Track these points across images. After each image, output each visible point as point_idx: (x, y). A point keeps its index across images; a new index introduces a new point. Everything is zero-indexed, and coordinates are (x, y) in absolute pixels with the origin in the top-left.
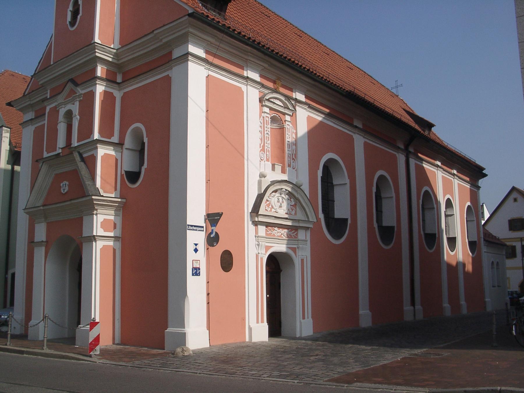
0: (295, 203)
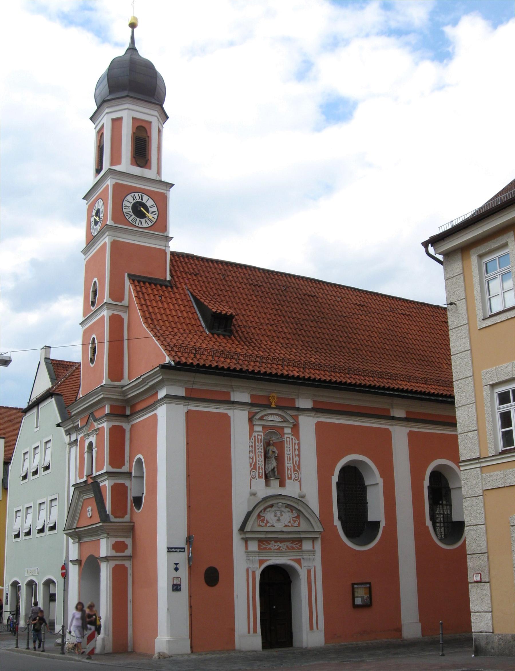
0: (298, 515)
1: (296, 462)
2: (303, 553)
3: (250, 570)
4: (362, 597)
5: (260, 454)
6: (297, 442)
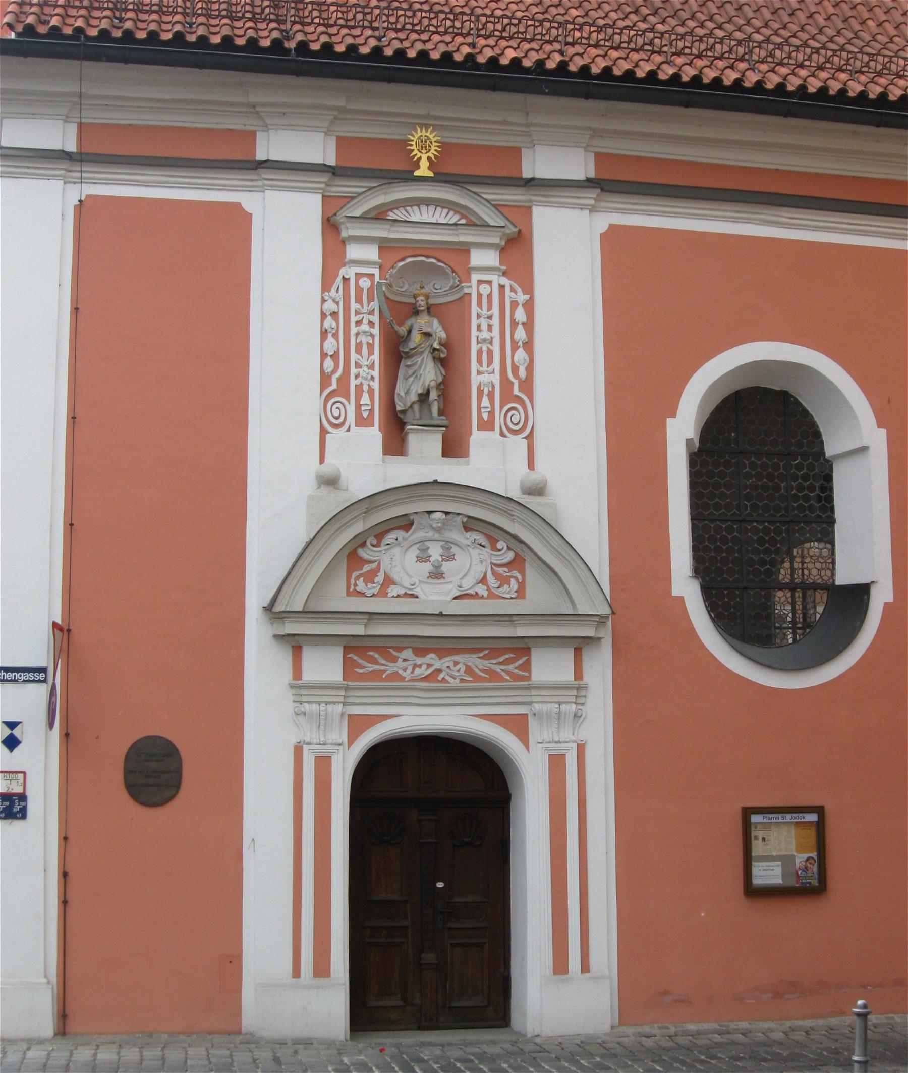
1: (515, 369)
2: (533, 692)
3: (306, 748)
4: (786, 861)
5: (364, 339)
6: (522, 297)
